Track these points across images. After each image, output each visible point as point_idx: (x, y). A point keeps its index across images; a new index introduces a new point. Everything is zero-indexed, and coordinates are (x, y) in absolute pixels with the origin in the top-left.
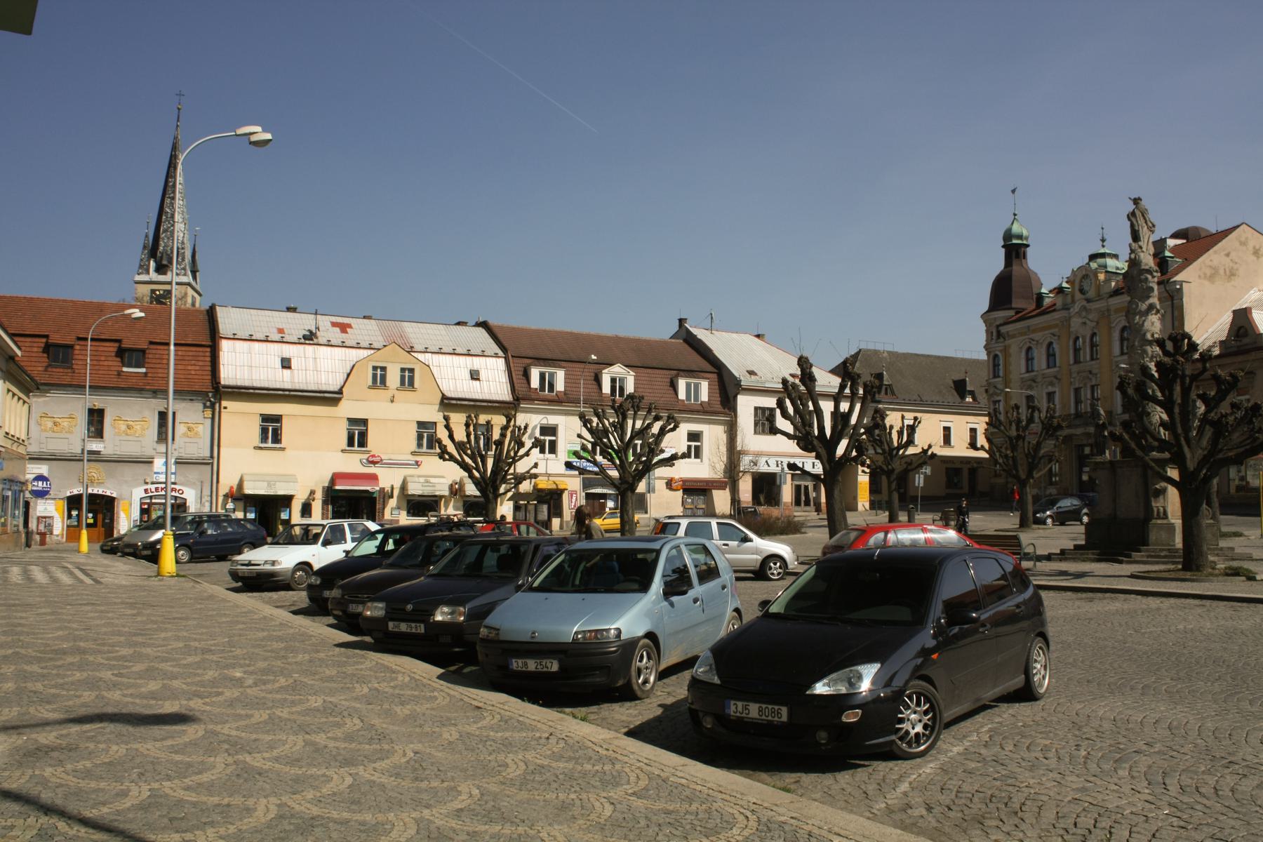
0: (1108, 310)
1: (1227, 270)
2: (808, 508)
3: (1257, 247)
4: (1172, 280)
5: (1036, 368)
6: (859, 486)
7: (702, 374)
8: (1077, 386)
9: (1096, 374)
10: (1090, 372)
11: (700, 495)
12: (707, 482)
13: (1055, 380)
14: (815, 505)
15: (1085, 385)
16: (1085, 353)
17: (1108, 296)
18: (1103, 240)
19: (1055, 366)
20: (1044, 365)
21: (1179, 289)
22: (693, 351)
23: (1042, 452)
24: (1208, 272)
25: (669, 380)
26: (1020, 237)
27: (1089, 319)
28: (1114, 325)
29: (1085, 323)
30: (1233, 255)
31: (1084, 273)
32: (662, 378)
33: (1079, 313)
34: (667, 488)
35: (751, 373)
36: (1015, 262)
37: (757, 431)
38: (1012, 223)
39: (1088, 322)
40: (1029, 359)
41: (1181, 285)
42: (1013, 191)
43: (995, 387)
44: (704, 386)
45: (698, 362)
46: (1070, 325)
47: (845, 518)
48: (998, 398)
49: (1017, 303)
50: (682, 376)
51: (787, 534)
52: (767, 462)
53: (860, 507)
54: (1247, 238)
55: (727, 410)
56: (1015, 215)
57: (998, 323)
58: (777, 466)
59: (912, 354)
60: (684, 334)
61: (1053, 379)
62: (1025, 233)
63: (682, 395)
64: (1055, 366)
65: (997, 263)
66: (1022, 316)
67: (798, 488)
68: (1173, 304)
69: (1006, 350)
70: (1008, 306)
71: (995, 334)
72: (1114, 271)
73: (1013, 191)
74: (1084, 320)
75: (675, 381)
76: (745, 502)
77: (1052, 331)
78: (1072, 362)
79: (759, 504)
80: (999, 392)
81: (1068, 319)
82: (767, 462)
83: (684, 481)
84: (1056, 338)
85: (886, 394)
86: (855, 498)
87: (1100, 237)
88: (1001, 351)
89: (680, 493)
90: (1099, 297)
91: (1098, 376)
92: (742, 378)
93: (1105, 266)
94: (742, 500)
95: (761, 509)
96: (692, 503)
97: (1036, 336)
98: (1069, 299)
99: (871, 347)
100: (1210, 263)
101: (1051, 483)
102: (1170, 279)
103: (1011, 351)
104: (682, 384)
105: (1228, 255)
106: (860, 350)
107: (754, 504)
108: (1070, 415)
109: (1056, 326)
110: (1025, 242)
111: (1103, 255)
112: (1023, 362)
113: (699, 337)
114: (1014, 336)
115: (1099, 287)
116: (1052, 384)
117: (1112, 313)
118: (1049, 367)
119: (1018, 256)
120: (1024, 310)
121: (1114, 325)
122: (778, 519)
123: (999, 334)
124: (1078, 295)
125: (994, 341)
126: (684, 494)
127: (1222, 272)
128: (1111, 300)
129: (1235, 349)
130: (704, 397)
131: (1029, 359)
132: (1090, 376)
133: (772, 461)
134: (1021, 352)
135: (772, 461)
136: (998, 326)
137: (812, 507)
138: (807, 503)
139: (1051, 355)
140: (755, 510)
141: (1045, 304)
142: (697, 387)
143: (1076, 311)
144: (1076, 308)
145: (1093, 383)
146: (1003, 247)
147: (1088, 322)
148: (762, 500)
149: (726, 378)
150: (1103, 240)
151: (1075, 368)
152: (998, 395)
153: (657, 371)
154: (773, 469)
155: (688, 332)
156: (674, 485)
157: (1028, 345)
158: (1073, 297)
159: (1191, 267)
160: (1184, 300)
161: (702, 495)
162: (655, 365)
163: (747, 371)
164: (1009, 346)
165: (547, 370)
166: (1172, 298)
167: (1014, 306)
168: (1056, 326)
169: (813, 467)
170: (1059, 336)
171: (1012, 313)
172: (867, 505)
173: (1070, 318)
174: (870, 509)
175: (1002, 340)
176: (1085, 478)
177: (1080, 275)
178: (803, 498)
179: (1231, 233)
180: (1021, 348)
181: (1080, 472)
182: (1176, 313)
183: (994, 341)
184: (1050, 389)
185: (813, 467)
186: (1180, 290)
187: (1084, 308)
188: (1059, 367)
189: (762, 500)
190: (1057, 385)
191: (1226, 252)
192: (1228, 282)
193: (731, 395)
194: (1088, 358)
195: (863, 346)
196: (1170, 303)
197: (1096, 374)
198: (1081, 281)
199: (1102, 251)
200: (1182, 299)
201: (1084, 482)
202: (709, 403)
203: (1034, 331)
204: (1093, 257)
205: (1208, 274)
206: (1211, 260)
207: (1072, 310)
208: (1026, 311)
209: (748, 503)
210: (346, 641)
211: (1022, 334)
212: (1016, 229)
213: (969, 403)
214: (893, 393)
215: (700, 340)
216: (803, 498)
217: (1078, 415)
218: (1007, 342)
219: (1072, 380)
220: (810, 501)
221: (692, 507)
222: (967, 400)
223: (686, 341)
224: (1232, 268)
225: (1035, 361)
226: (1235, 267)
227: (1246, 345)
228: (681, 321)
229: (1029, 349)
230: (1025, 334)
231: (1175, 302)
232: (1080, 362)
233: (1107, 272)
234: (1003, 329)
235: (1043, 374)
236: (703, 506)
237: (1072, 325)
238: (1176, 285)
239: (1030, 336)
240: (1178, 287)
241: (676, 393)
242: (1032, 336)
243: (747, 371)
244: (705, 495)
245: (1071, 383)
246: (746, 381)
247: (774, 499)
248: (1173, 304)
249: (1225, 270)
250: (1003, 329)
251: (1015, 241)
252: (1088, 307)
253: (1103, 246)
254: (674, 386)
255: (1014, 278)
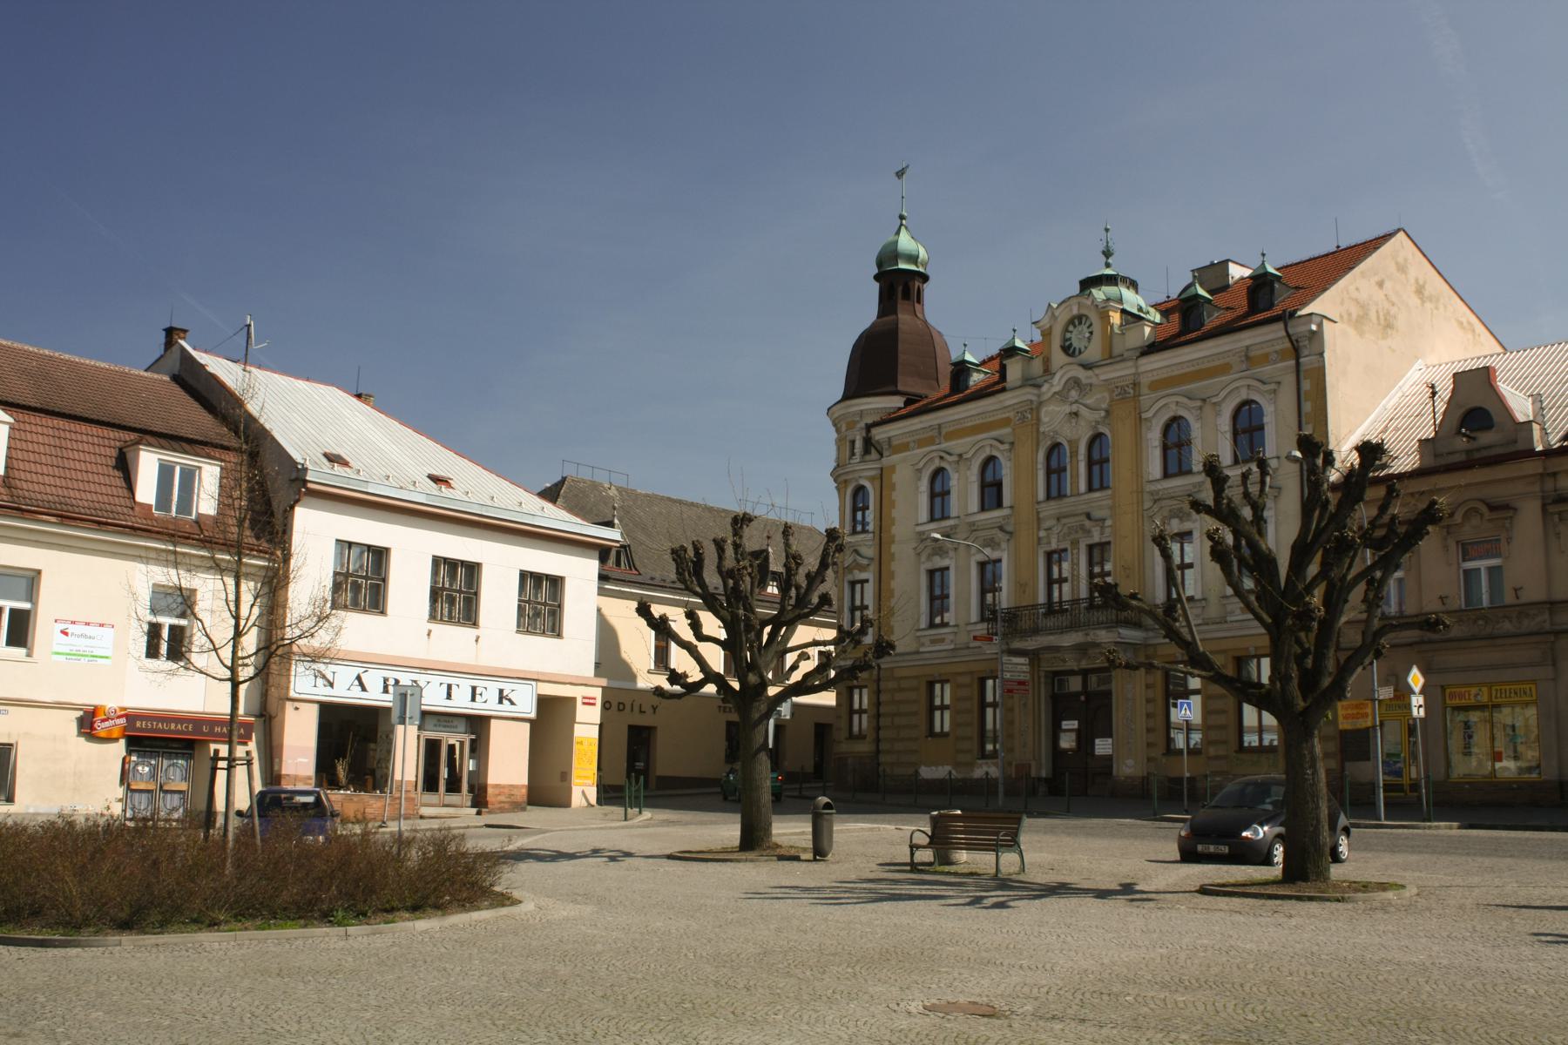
0: (1136, 385)
1: (1381, 314)
2: (453, 798)
3: (1421, 282)
4: (1299, 313)
5: (954, 513)
6: (576, 747)
7: (207, 450)
8: (1054, 546)
9: (1103, 520)
10: (1088, 516)
11: (177, 756)
12: (197, 722)
13: (1000, 535)
14: (471, 789)
15: (1075, 543)
16: (1076, 476)
17: (1138, 354)
18: (1107, 253)
19: (999, 505)
20: (974, 505)
21: (1314, 333)
22: (191, 401)
23: (1343, 619)
24: (1355, 311)
25: (114, 453)
26: (913, 259)
27: (1085, 405)
28: (1149, 415)
29: (1076, 414)
30: (1388, 285)
31: (1075, 311)
32: (97, 445)
33: (1062, 396)
34: (80, 734)
35: (332, 458)
36: (902, 305)
37: (341, 600)
38: (898, 233)
39: (1084, 411)
40: (939, 494)
41: (1320, 325)
42: (900, 174)
43: (856, 552)
44: (210, 475)
45: (193, 418)
46: (1038, 419)
47: (1328, 870)
48: (863, 576)
49: (906, 383)
50: (150, 445)
51: (440, 908)
52: (359, 678)
53: (577, 799)
54: (1406, 260)
55: (265, 545)
56: (902, 217)
57: (870, 421)
58: (386, 691)
59: (662, 498)
60: (173, 360)
61: (996, 531)
62: (923, 254)
63: (146, 490)
64: (999, 505)
65: (864, 310)
66: (916, 406)
67: (432, 748)
68: (1298, 364)
69: (882, 477)
70: (891, 388)
71: (859, 445)
72: (1135, 311)
73: (900, 174)
74: (1074, 408)
75: (129, 456)
76: (296, 778)
77: (994, 433)
78: (1041, 495)
79: (334, 784)
80: (865, 562)
81: (1036, 408)
82: (359, 678)
83: (131, 717)
84: (1007, 446)
85: (618, 563)
86: (565, 776)
87: (1102, 247)
88: (871, 479)
89: (120, 747)
90: (1111, 357)
91: (1108, 523)
92: (308, 465)
93: (1120, 301)
94: (284, 772)
95: (337, 798)
96: (153, 775)
97: (957, 445)
98: (1037, 367)
99: (585, 474)
100: (1355, 294)
101: (983, 755)
102: (1296, 311)
103: (896, 478)
104: (148, 463)
105: (1381, 284)
106: (564, 480)
107: (319, 784)
108: (1035, 606)
109: (1006, 422)
110: (921, 269)
111: (1111, 280)
112: (924, 499)
113: (210, 369)
114: (904, 447)
115: (1109, 339)
116: (992, 543)
117: (1144, 390)
118: (983, 509)
119: (907, 295)
120: (921, 397)
121: (1149, 415)
122: (401, 841)
123: (868, 444)
124: (1058, 357)
125: (857, 458)
126: (129, 752)
127: (1373, 315)
128: (1144, 360)
129: (1463, 457)
130: (206, 503)
131: (939, 494)
132: (1087, 523)
133: (374, 679)
134: (919, 479)
135: (374, 679)
136: (869, 427)
137: (465, 796)
138: (453, 786)
139: (991, 493)
140: (318, 801)
141: (971, 383)
142: (189, 476)
143: (1057, 389)
144: (1057, 383)
145: (1096, 539)
146: (877, 278)
147: (1084, 411)
148: (341, 772)
149: (272, 469)
150: (1107, 253)
151: (1052, 508)
152: (863, 568)
153: (84, 428)
154: (375, 696)
155: (187, 359)
156: (101, 728)
157: (937, 463)
158: (1047, 362)
159: (1327, 293)
160: (1326, 355)
161: (183, 756)
162: (78, 411)
163: (326, 455)
164: (892, 468)
165: (180, 460)
166: (1296, 352)
167: (900, 388)
168: (1006, 422)
169: (473, 699)
170: (1012, 444)
171: (898, 402)
172: (592, 794)
173: (1040, 404)
174: (599, 802)
175: (874, 455)
176: (1067, 742)
177: (1063, 317)
178: (444, 773)
179: (1376, 248)
180: (919, 471)
181: (1056, 731)
182: (1306, 385)
183: (857, 458)
184: (989, 553)
185: (473, 699)
186: (1317, 336)
187: (1076, 382)
188: (1011, 507)
189: (341, 772)
190: (1004, 545)
191: (1377, 278)
192: (1384, 338)
193: (278, 506)
194: (1083, 486)
195: (570, 471)
196: (1292, 362)
197: (1103, 520)
198: (1066, 330)
199: (1109, 272)
200: (1321, 354)
201: (1065, 751)
202: (217, 521)
203: (951, 436)
204: (1088, 284)
205: (1354, 316)
206: (1357, 289)
207: (1044, 389)
208: (929, 400)
209: (306, 779)
210: (1280, 568)
211: (921, 443)
212: (905, 242)
213: (773, 595)
214: (631, 564)
215: (213, 377)
216: (444, 773)
217: (1051, 609)
218: (886, 461)
219: (1042, 534)
220: (459, 780)
221: (151, 787)
222: (770, 590)
223: (176, 379)
224: (1388, 313)
225: (954, 499)
226: (1394, 310)
227: (1490, 447)
228: (171, 333)
229: (939, 473)
230: (930, 441)
231: (1302, 360)
232: (1065, 496)
233: (1124, 311)
234: (879, 434)
235: (973, 524)
236: (183, 786)
237: (1045, 419)
238: (1311, 322)
239: (944, 445)
240: (1314, 327)
241: (130, 485)
242: (944, 445)
243: (326, 455)
244: (189, 757)
245: (1039, 539)
246: (320, 473)
247: (373, 773)
248: (1298, 364)
249: (1377, 312)
250: (879, 434)
251: (902, 266)
252: (1084, 381)
253: (1108, 265)
254: (125, 468)
255: (901, 336)
